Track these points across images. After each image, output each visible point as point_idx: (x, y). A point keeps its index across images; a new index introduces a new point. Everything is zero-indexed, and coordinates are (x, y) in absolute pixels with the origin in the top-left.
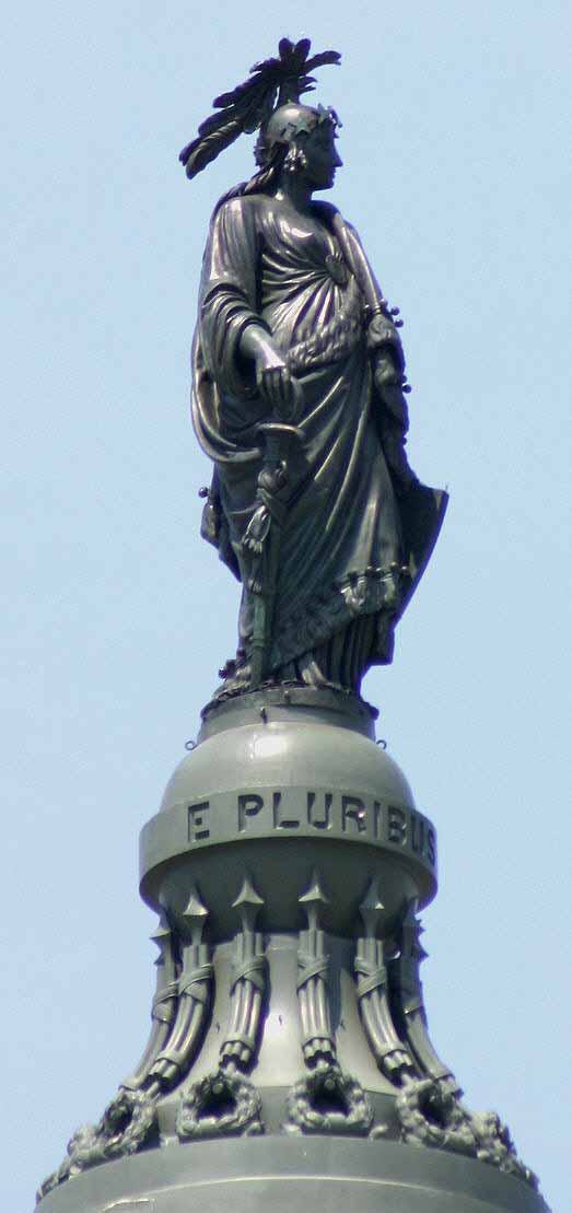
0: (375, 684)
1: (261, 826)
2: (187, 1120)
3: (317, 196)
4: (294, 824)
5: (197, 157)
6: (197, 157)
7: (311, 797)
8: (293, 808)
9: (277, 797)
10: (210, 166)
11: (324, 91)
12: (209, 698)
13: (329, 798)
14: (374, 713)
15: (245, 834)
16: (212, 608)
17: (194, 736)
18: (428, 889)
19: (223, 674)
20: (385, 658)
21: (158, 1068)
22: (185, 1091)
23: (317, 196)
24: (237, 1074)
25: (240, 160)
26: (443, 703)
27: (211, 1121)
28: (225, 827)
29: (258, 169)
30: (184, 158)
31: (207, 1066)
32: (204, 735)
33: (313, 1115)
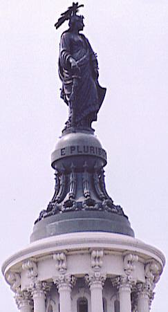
0: (94, 125)
1: (75, 153)
2: (63, 209)
3: (80, 32)
4: (81, 152)
5: (58, 25)
6: (58, 25)
7: (84, 147)
8: (81, 149)
9: (78, 147)
10: (60, 27)
11: (132, 272)
12: (63, 128)
13: (88, 147)
14: (94, 130)
15: (73, 154)
16: (64, 112)
17: (61, 135)
18: (106, 163)
19: (66, 123)
20: (96, 120)
21: (57, 199)
22: (63, 203)
23: (80, 32)
24: (73, 200)
25: (65, 26)
26: (104, 129)
27: (68, 209)
28: (68, 153)
29: (104, 168)
30: (55, 25)
31: (67, 198)
32: (63, 135)
33: (87, 207)
